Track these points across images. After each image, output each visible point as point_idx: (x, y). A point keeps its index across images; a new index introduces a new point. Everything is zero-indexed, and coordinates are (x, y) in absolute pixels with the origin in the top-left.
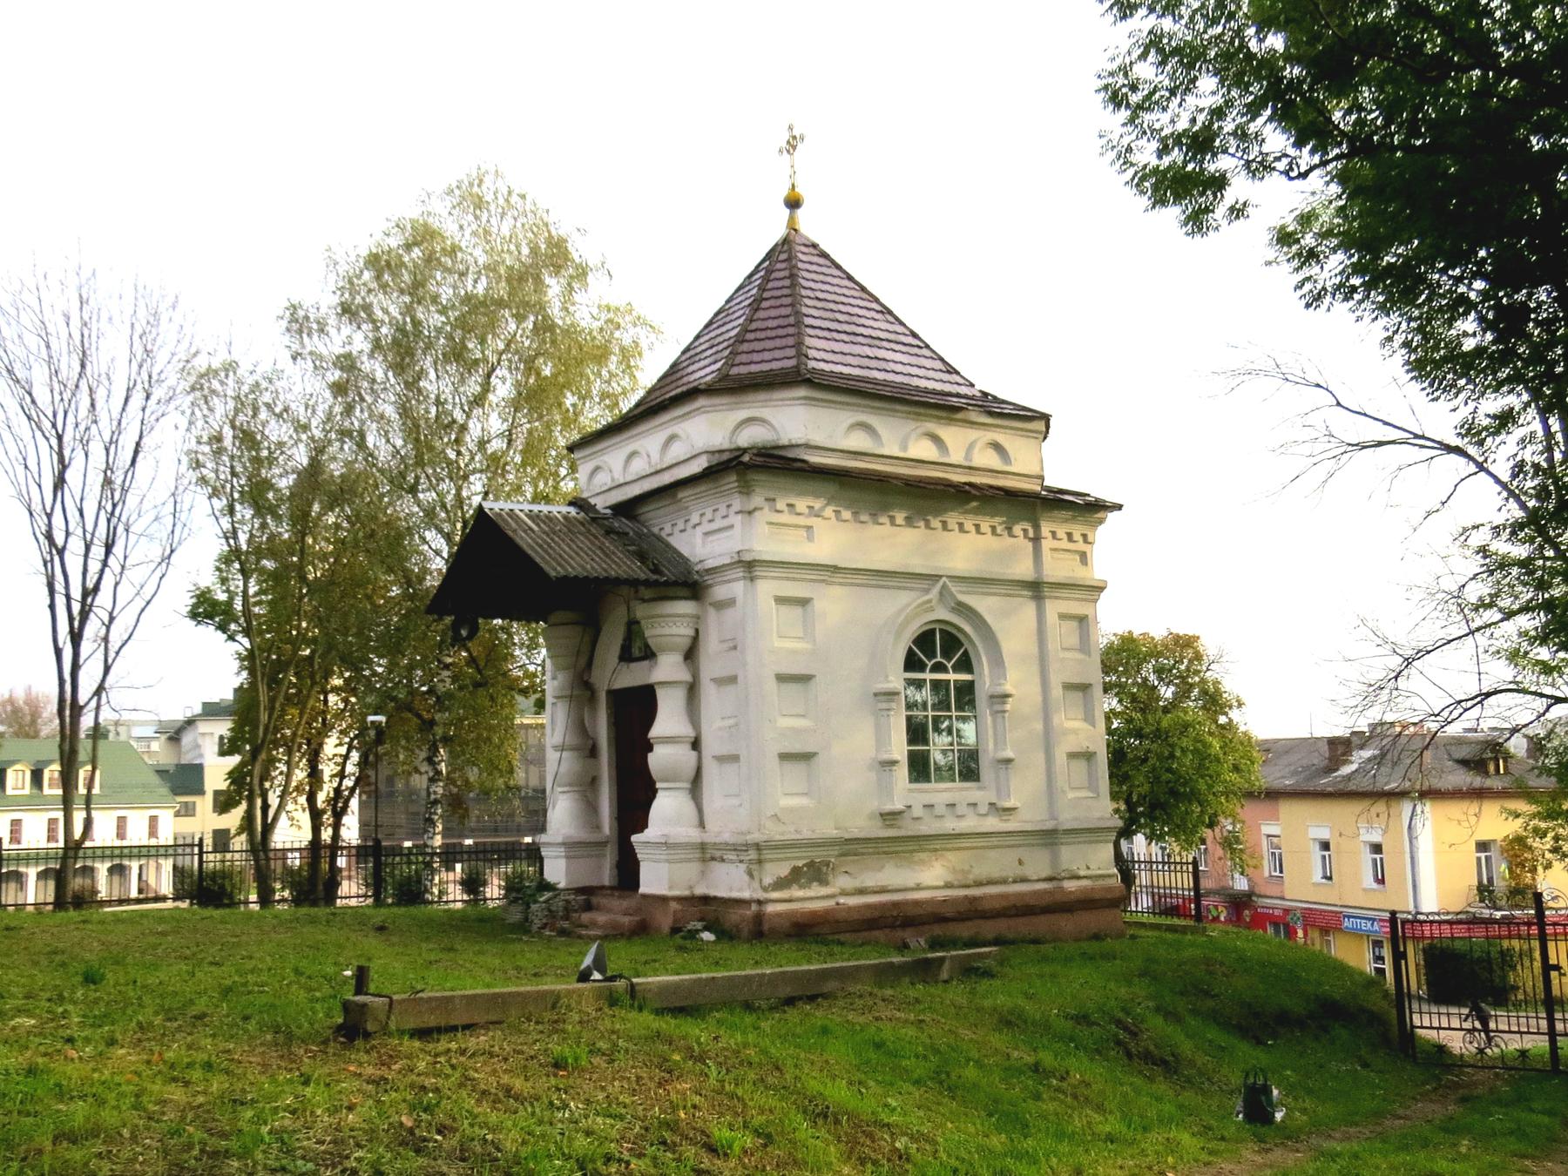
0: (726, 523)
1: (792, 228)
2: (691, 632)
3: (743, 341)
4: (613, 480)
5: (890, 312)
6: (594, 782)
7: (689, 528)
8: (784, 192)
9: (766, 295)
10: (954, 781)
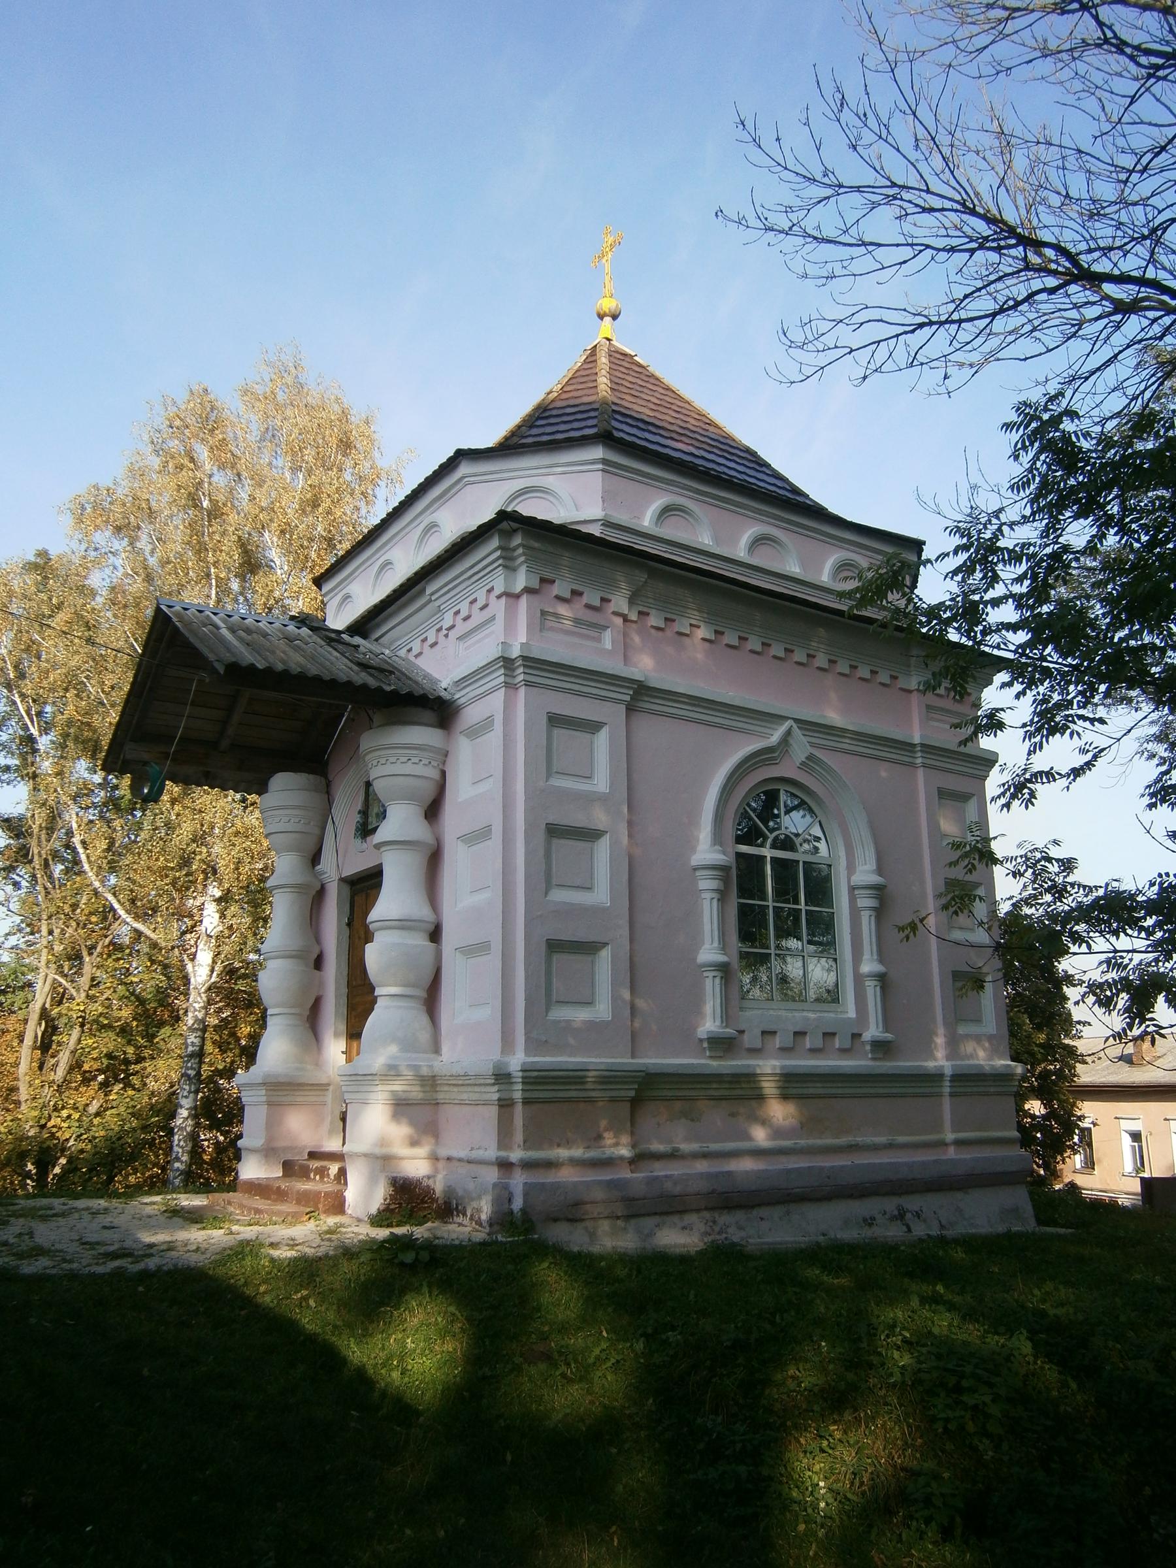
0: (487, 614)
2: (434, 774)
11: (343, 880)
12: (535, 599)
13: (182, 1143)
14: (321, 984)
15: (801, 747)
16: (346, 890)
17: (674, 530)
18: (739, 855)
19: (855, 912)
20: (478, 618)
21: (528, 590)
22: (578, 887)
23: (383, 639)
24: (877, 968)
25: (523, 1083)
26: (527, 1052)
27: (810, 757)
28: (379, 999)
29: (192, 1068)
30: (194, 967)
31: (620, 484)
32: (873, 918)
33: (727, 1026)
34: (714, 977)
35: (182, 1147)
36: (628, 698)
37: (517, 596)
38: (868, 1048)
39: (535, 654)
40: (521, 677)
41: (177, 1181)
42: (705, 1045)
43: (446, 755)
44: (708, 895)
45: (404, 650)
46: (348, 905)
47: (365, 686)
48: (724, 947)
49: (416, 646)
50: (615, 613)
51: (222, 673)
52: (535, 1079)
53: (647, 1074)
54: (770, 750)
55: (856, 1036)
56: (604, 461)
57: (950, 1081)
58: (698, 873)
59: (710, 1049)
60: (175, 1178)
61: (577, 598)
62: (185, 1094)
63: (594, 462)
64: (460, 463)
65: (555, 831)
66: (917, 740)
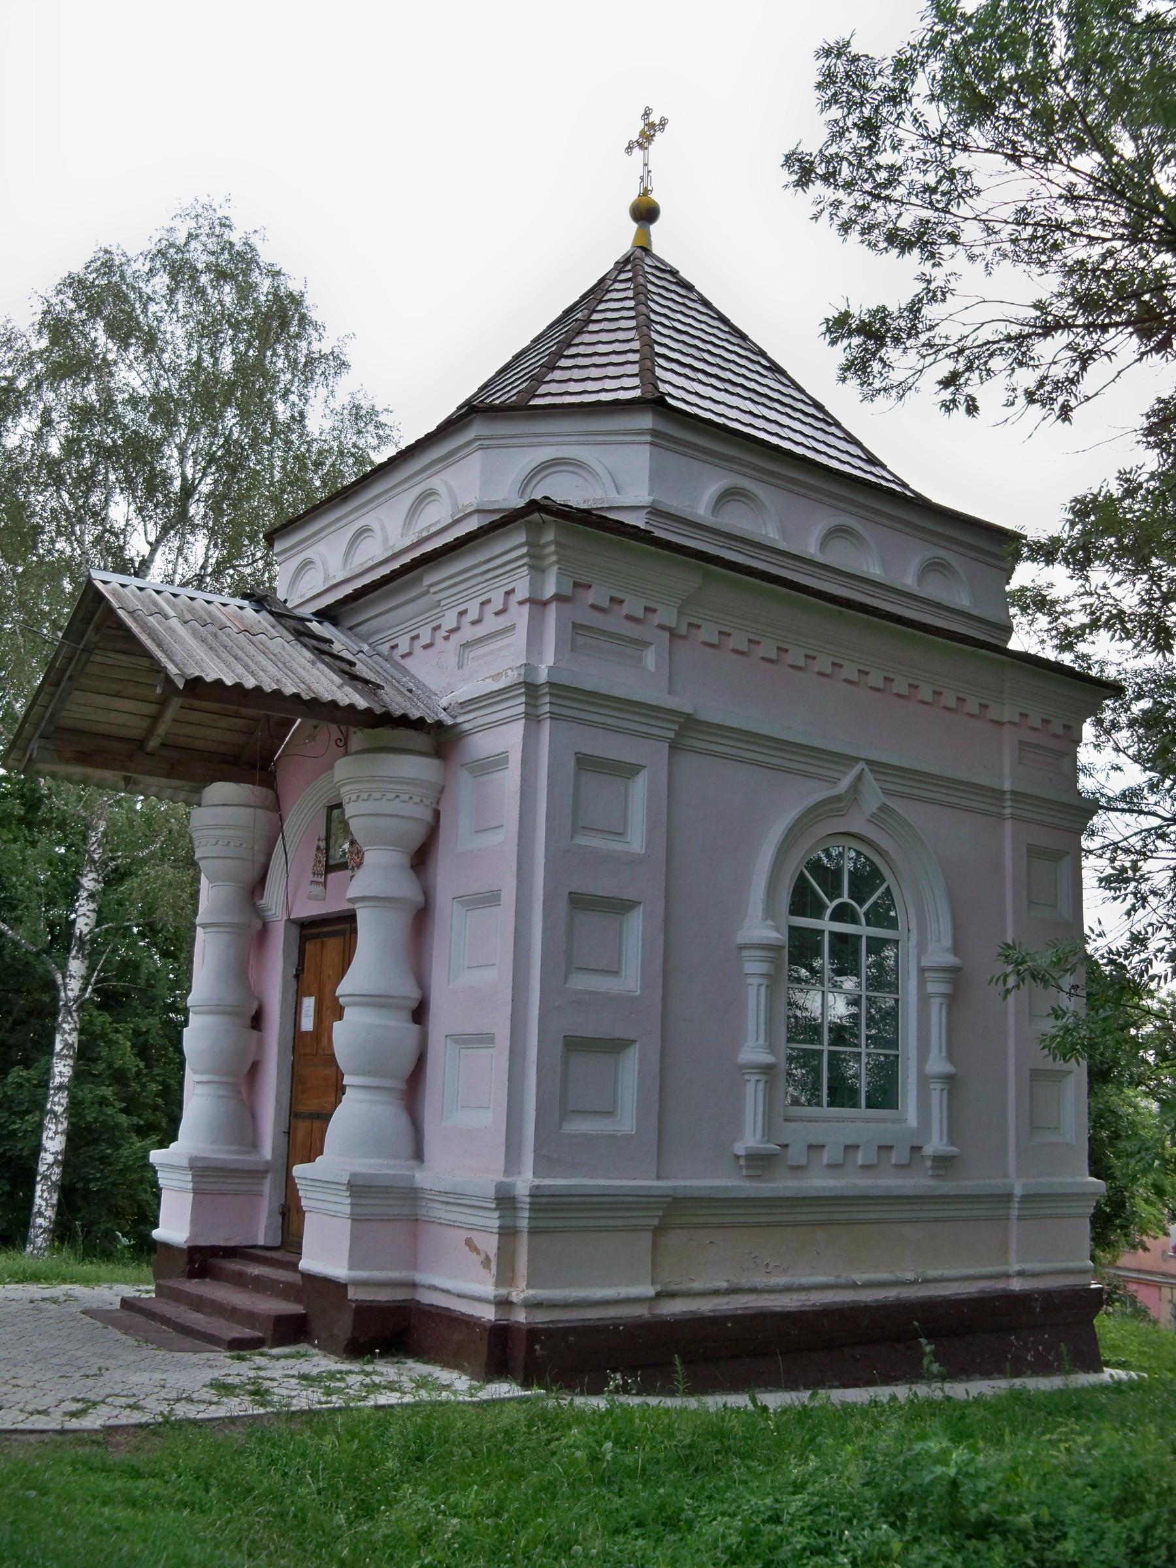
0: (502, 622)
1: (644, 247)
2: (427, 815)
3: (554, 368)
4: (326, 579)
5: (782, 372)
6: (253, 1071)
7: (439, 641)
8: (632, 195)
9: (595, 317)
10: (819, 1104)
11: (290, 921)
12: (567, 607)
13: (46, 1195)
14: (261, 1045)
15: (873, 797)
16: (295, 931)
17: (736, 520)
18: (793, 929)
19: (924, 999)
20: (492, 623)
21: (558, 598)
22: (603, 971)
23: (359, 628)
24: (947, 1068)
25: (530, 1210)
26: (535, 1175)
27: (884, 808)
28: (348, 1090)
29: (59, 1104)
30: (64, 978)
31: (675, 462)
32: (944, 1007)
33: (769, 1141)
34: (758, 1081)
35: (46, 1200)
36: (672, 735)
37: (545, 604)
38: (929, 1163)
39: (563, 680)
40: (547, 708)
41: (39, 1241)
42: (742, 1162)
43: (442, 791)
44: (755, 981)
45: (387, 646)
46: (296, 952)
47: (351, 706)
48: (771, 1047)
49: (404, 645)
50: (661, 627)
51: (181, 687)
52: (543, 1202)
53: (675, 1199)
54: (837, 798)
55: (916, 1149)
56: (654, 433)
57: (1019, 1202)
58: (745, 953)
59: (748, 1167)
60: (37, 1236)
61: (616, 607)
62: (51, 1134)
63: (640, 432)
64: (470, 423)
65: (580, 902)
66: (1007, 786)
